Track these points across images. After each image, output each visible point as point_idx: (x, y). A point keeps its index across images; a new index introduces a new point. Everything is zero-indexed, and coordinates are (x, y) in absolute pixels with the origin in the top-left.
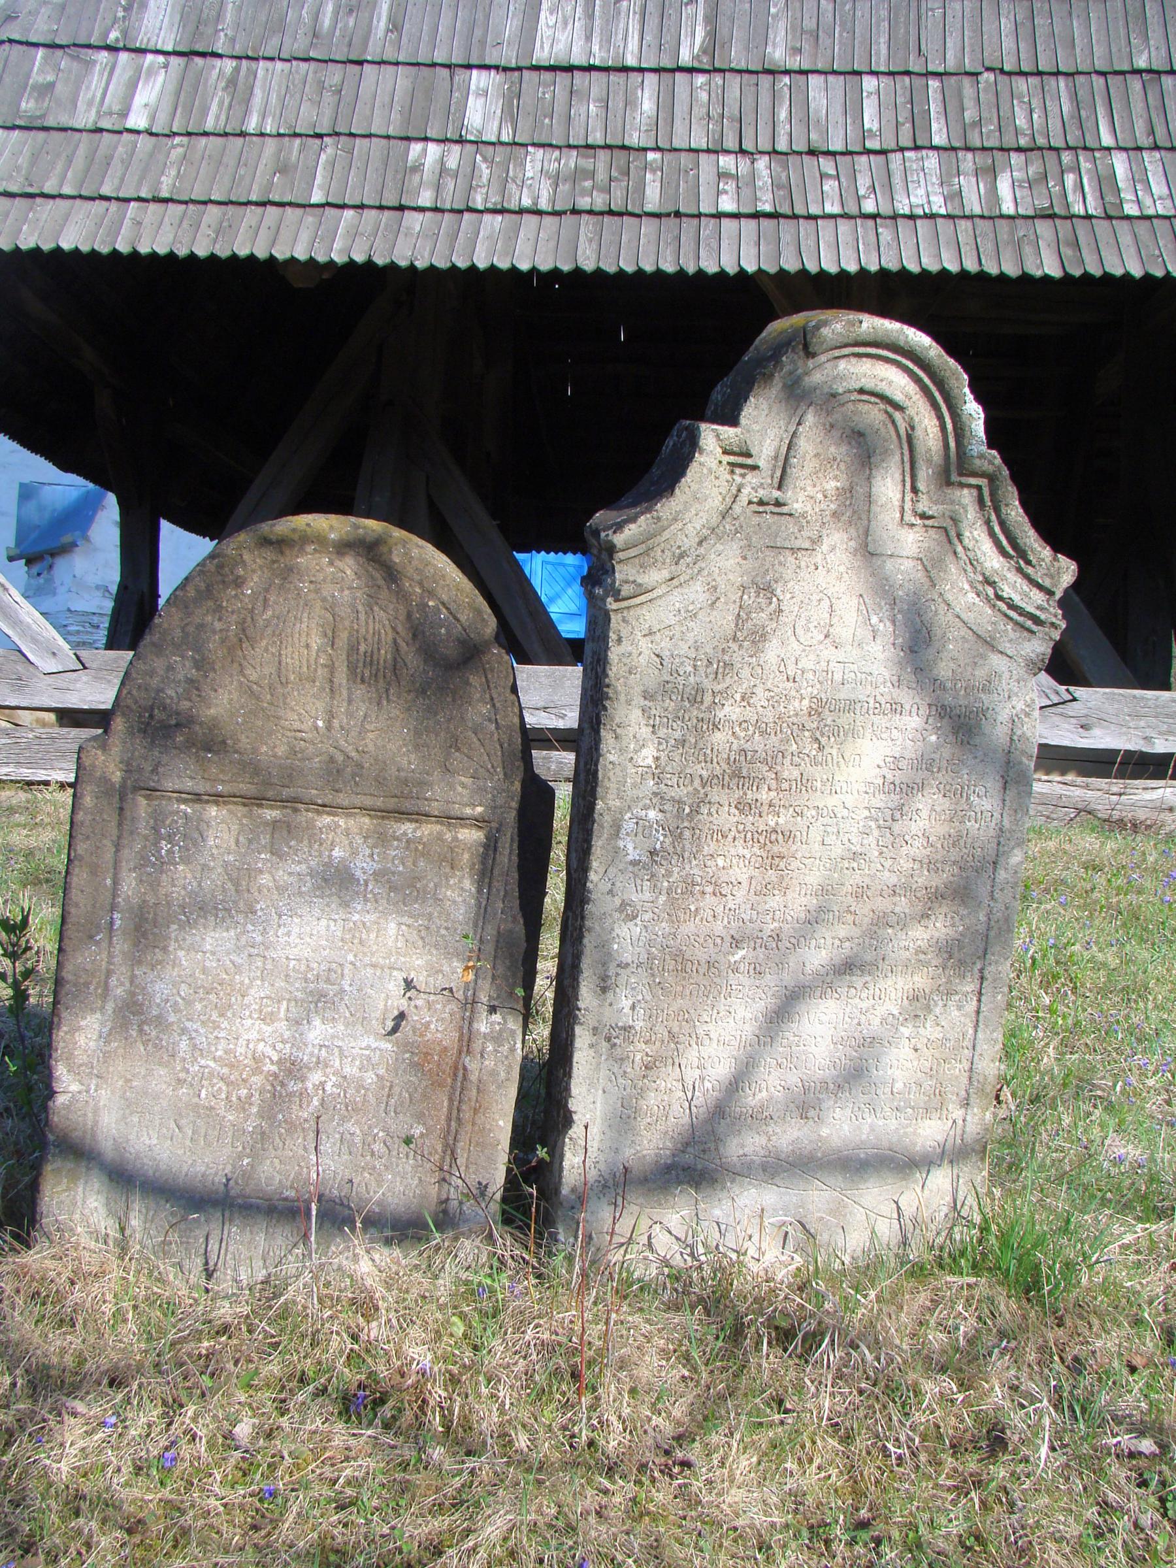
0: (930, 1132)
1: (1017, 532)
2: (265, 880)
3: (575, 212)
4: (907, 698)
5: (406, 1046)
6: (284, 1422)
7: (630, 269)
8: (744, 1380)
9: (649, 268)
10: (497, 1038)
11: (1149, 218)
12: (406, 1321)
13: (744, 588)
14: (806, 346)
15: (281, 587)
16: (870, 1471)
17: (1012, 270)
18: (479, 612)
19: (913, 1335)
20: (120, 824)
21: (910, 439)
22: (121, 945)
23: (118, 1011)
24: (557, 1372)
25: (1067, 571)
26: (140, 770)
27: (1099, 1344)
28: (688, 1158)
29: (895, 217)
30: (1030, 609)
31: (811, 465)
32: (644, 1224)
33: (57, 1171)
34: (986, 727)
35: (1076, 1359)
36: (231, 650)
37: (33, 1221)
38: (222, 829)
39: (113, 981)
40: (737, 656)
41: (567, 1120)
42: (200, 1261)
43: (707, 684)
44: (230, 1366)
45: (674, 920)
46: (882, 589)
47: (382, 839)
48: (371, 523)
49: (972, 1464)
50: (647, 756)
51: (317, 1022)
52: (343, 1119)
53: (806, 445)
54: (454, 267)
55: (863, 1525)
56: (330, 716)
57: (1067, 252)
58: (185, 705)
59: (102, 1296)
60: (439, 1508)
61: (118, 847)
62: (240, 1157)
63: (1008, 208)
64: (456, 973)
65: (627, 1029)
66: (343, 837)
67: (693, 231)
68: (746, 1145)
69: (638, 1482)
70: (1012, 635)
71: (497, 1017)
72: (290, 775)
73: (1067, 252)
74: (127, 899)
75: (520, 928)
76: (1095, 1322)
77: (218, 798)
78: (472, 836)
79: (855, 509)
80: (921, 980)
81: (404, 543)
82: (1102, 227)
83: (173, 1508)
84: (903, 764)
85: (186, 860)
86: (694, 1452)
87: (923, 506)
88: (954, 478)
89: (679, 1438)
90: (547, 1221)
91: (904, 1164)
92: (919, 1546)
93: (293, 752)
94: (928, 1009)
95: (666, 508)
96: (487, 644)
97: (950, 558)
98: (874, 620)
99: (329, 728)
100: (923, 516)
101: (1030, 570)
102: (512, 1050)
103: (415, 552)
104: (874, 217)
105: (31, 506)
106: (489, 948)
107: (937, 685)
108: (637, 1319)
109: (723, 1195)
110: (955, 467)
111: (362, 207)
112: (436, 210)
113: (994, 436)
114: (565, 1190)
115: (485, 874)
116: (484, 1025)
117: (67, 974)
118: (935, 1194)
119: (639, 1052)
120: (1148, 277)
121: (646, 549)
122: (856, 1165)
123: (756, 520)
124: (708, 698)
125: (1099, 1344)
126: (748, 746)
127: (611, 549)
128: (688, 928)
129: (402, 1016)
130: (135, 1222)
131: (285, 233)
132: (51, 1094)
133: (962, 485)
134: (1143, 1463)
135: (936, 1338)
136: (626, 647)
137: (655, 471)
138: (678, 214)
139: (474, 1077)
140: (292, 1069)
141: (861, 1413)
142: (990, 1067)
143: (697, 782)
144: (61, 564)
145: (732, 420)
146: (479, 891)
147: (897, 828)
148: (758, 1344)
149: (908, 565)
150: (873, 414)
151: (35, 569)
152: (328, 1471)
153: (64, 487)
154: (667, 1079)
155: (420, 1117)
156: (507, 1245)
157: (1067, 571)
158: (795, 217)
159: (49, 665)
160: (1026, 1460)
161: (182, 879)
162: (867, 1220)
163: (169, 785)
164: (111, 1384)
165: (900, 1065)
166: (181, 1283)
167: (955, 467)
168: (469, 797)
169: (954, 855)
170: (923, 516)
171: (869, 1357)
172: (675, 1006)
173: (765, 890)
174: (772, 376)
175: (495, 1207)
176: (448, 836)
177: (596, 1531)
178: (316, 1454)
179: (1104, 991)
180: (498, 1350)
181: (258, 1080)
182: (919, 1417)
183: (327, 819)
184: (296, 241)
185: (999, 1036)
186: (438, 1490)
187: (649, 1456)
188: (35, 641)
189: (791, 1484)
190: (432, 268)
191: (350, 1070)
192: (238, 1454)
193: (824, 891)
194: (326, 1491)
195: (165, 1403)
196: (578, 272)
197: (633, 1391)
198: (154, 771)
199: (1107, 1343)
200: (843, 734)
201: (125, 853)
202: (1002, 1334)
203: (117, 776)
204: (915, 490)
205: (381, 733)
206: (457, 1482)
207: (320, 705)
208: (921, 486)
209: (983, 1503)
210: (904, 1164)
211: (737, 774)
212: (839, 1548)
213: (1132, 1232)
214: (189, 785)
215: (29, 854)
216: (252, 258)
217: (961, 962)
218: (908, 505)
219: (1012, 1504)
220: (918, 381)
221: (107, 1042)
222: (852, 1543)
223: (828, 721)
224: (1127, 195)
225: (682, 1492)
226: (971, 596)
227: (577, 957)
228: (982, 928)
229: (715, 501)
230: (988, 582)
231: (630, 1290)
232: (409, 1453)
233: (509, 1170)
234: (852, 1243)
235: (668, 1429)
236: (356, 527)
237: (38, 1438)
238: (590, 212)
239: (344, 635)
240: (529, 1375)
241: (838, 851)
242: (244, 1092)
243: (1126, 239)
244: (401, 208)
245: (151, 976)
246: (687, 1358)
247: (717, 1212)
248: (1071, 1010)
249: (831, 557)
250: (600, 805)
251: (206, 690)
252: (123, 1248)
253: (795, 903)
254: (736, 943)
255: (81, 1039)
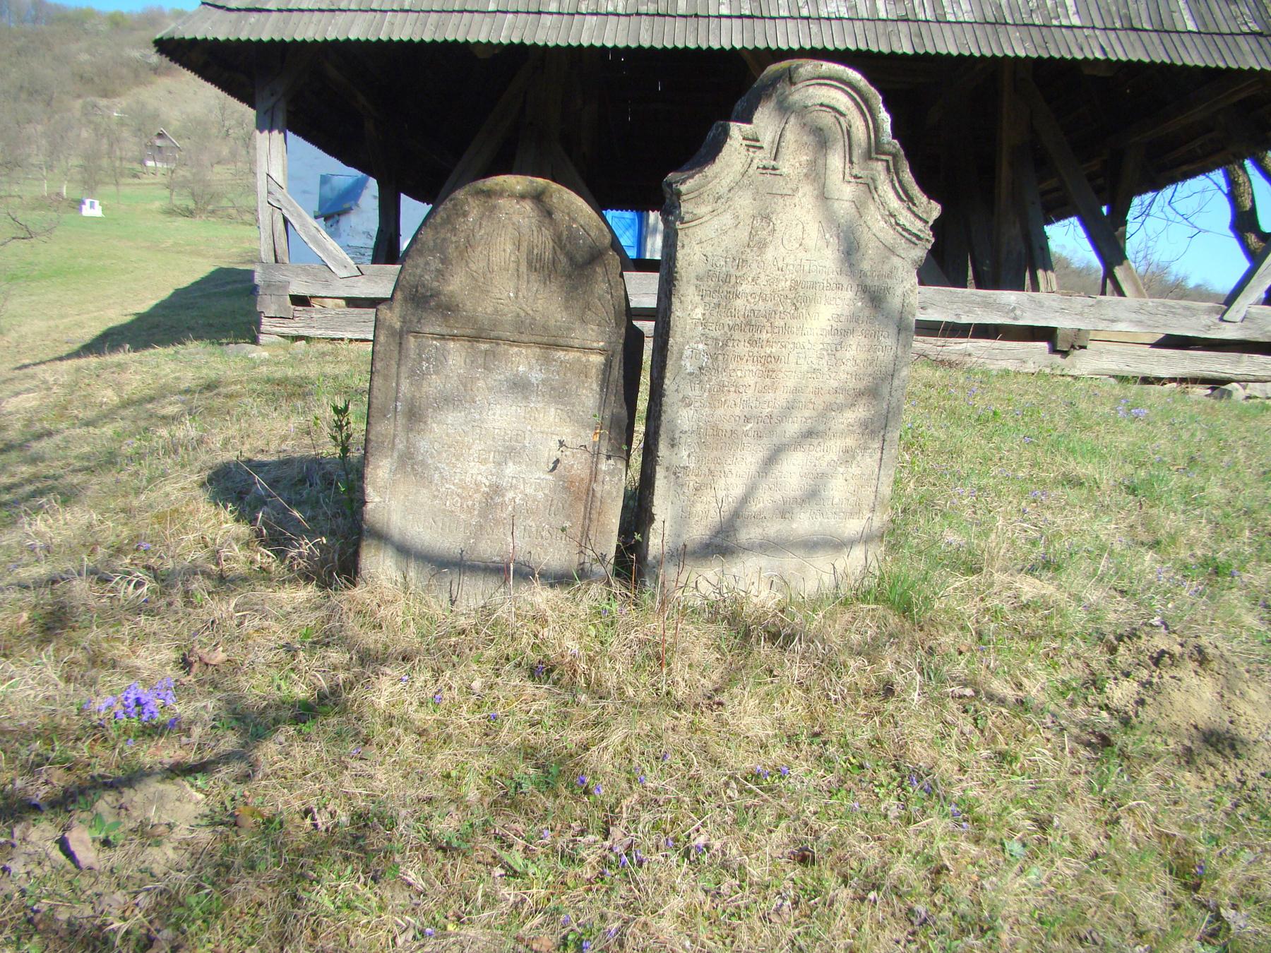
0: (854, 527)
1: (908, 187)
2: (481, 384)
3: (638, 14)
4: (845, 280)
5: (561, 478)
6: (499, 680)
7: (670, 46)
8: (750, 660)
9: (680, 46)
10: (611, 473)
11: (960, 23)
12: (564, 627)
13: (754, 217)
14: (790, 79)
15: (489, 217)
16: (820, 707)
17: (885, 50)
18: (601, 230)
19: (842, 636)
20: (400, 352)
21: (848, 132)
22: (401, 421)
23: (400, 457)
24: (648, 656)
25: (935, 210)
26: (411, 321)
27: (942, 640)
28: (718, 541)
29: (819, 19)
30: (915, 231)
31: (792, 147)
32: (693, 577)
33: (369, 545)
34: (889, 298)
35: (930, 648)
36: (461, 253)
37: (356, 573)
38: (456, 356)
39: (397, 441)
40: (750, 255)
41: (651, 519)
42: (447, 595)
43: (733, 271)
44: (467, 651)
45: (712, 406)
46: (830, 219)
47: (547, 361)
48: (540, 180)
49: (875, 703)
50: (698, 313)
51: (510, 464)
52: (525, 518)
53: (790, 136)
54: (570, 46)
55: (816, 735)
56: (517, 291)
57: (916, 40)
58: (436, 284)
59: (395, 613)
60: (585, 726)
61: (399, 365)
62: (469, 538)
63: (883, 15)
64: (589, 437)
65: (685, 468)
66: (523, 362)
67: (705, 26)
68: (748, 534)
69: (694, 713)
70: (904, 246)
71: (611, 462)
72: (495, 325)
73: (916, 40)
74: (404, 395)
75: (624, 413)
76: (941, 628)
77: (454, 337)
78: (597, 359)
79: (816, 174)
80: (850, 442)
81: (559, 191)
82: (934, 26)
83: (441, 724)
84: (842, 319)
85: (437, 373)
86: (724, 697)
87: (856, 171)
88: (874, 155)
89: (716, 690)
90: (640, 574)
91: (837, 545)
92: (847, 745)
93: (496, 311)
94: (854, 457)
95: (710, 170)
96: (606, 250)
97: (870, 201)
98: (828, 236)
99: (517, 297)
100: (856, 177)
101: (915, 209)
102: (620, 480)
103: (565, 196)
104: (807, 18)
105: (327, 188)
106: (607, 422)
107: (862, 274)
108: (690, 627)
109: (738, 560)
110: (874, 150)
111: (517, 12)
112: (559, 13)
113: (896, 133)
114: (650, 558)
115: (605, 382)
116: (604, 466)
117: (372, 437)
118: (854, 561)
119: (692, 481)
120: (960, 55)
121: (698, 194)
122: (812, 545)
123: (761, 177)
124: (733, 280)
125: (942, 640)
126: (755, 308)
127: (679, 194)
128: (720, 411)
129: (558, 461)
130: (412, 574)
131: (474, 28)
132: (365, 503)
133: (878, 160)
134: (965, 701)
135: (855, 638)
136: (687, 250)
137: (703, 150)
138: (696, 16)
139: (598, 495)
140: (496, 490)
141: (815, 677)
142: (886, 490)
143: (726, 328)
144: (343, 219)
145: (748, 120)
146: (602, 390)
147: (838, 355)
148: (758, 642)
149: (847, 205)
150: (827, 119)
151: (329, 223)
152: (524, 707)
153: (345, 175)
154: (708, 496)
155: (568, 517)
156: (617, 587)
157: (935, 210)
158: (763, 18)
159: (343, 273)
160: (904, 700)
161: (434, 384)
162: (817, 575)
163: (427, 330)
164: (403, 660)
165: (838, 490)
166: (437, 606)
167: (874, 150)
168: (592, 345)
169: (870, 370)
170: (856, 177)
171: (820, 647)
172: (712, 456)
173: (765, 389)
174: (771, 95)
175: (610, 567)
176: (584, 359)
177: (671, 737)
178: (517, 697)
179: (939, 453)
180: (614, 645)
181: (478, 496)
182: (847, 679)
183: (516, 349)
184: (480, 32)
185: (892, 472)
186: (585, 717)
187: (699, 700)
188: (335, 259)
189: (776, 714)
190: (557, 46)
191: (529, 491)
192: (475, 697)
193: (796, 390)
194: (524, 716)
195: (433, 670)
196: (640, 48)
197: (690, 666)
198: (419, 322)
199: (947, 640)
200: (808, 301)
201: (403, 369)
202: (891, 635)
203: (398, 325)
204: (851, 162)
205: (546, 304)
206: (595, 713)
207: (512, 284)
208: (855, 159)
209: (881, 723)
210: (837, 545)
211: (749, 324)
212: (804, 747)
213: (960, 581)
214: (438, 330)
215: (336, 378)
216: (456, 41)
217: (872, 432)
218: (847, 171)
219: (896, 723)
220: (853, 99)
221: (395, 474)
222: (810, 745)
223: (800, 296)
224: (949, 10)
225: (718, 719)
226: (882, 223)
227: (657, 428)
228: (884, 412)
229: (738, 167)
230: (892, 215)
231: (688, 612)
232: (568, 698)
233: (618, 547)
234: (809, 587)
235: (710, 686)
236: (531, 182)
237: (368, 685)
238: (647, 14)
239: (525, 244)
240: (633, 657)
241: (805, 368)
242: (470, 503)
243: (948, 34)
244: (539, 13)
245: (418, 437)
246: (719, 648)
247: (734, 570)
248: (921, 463)
249: (804, 200)
250: (671, 341)
251: (447, 275)
252: (406, 587)
253: (781, 398)
254: (747, 420)
255: (380, 473)
